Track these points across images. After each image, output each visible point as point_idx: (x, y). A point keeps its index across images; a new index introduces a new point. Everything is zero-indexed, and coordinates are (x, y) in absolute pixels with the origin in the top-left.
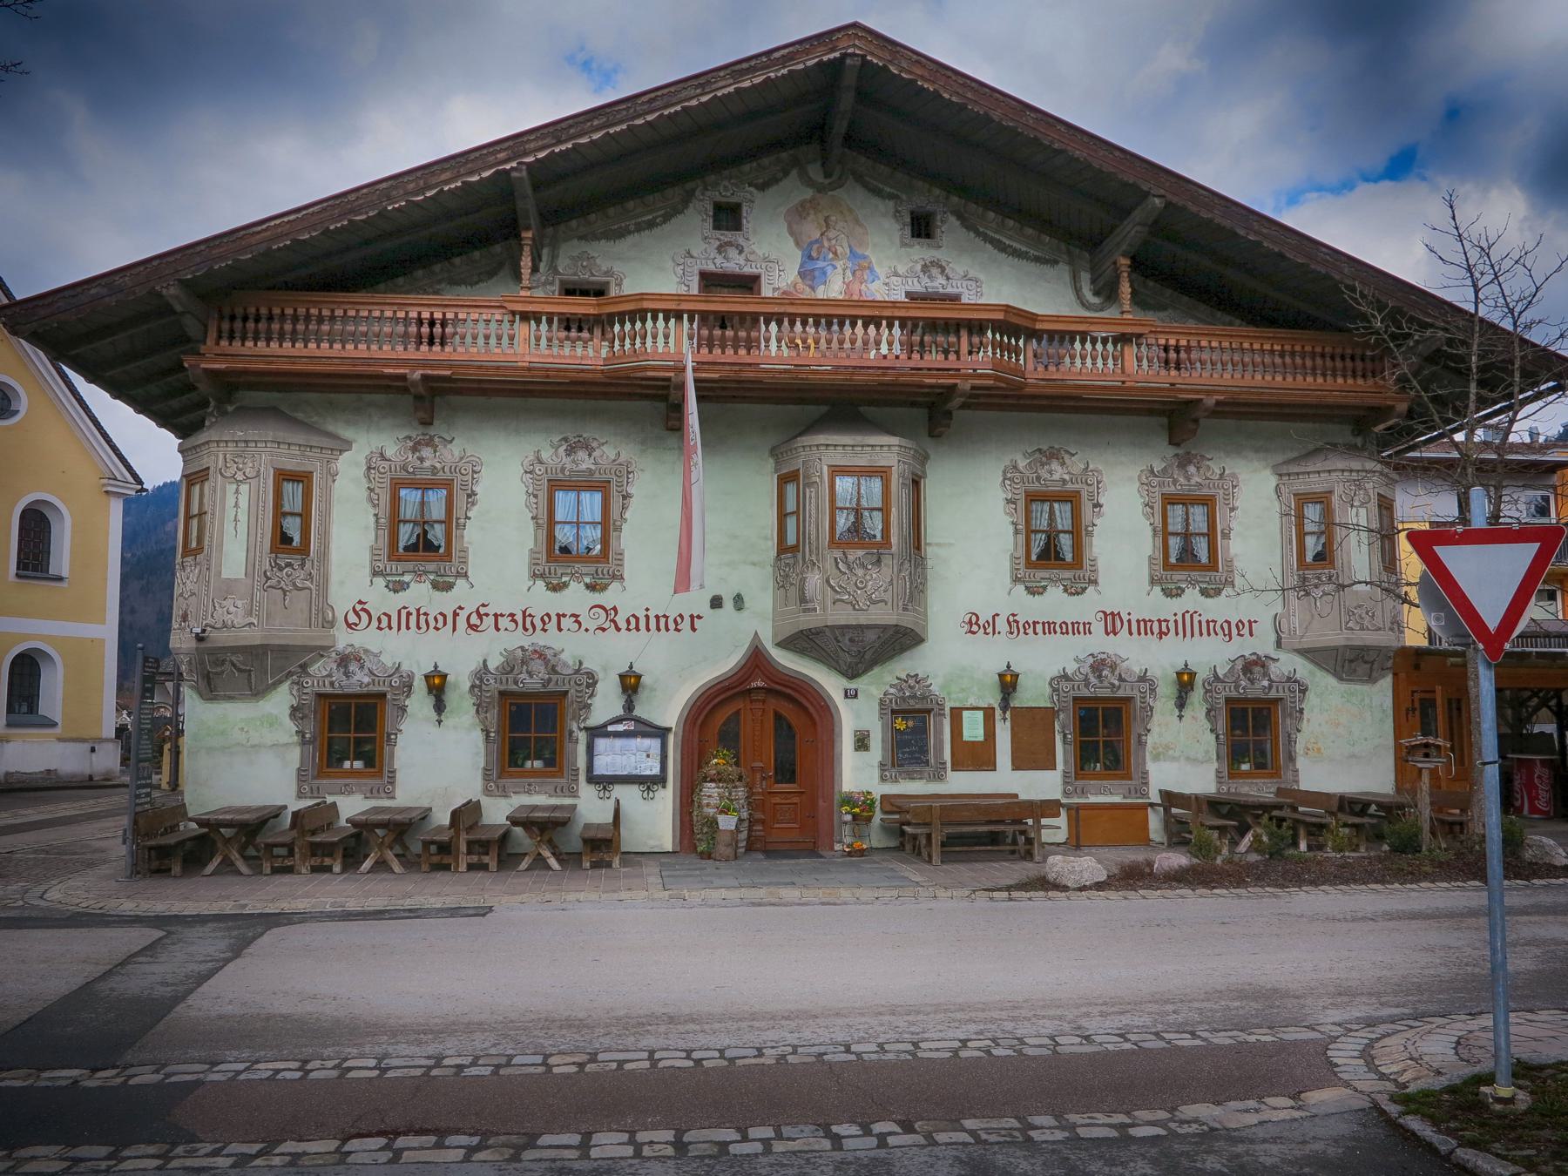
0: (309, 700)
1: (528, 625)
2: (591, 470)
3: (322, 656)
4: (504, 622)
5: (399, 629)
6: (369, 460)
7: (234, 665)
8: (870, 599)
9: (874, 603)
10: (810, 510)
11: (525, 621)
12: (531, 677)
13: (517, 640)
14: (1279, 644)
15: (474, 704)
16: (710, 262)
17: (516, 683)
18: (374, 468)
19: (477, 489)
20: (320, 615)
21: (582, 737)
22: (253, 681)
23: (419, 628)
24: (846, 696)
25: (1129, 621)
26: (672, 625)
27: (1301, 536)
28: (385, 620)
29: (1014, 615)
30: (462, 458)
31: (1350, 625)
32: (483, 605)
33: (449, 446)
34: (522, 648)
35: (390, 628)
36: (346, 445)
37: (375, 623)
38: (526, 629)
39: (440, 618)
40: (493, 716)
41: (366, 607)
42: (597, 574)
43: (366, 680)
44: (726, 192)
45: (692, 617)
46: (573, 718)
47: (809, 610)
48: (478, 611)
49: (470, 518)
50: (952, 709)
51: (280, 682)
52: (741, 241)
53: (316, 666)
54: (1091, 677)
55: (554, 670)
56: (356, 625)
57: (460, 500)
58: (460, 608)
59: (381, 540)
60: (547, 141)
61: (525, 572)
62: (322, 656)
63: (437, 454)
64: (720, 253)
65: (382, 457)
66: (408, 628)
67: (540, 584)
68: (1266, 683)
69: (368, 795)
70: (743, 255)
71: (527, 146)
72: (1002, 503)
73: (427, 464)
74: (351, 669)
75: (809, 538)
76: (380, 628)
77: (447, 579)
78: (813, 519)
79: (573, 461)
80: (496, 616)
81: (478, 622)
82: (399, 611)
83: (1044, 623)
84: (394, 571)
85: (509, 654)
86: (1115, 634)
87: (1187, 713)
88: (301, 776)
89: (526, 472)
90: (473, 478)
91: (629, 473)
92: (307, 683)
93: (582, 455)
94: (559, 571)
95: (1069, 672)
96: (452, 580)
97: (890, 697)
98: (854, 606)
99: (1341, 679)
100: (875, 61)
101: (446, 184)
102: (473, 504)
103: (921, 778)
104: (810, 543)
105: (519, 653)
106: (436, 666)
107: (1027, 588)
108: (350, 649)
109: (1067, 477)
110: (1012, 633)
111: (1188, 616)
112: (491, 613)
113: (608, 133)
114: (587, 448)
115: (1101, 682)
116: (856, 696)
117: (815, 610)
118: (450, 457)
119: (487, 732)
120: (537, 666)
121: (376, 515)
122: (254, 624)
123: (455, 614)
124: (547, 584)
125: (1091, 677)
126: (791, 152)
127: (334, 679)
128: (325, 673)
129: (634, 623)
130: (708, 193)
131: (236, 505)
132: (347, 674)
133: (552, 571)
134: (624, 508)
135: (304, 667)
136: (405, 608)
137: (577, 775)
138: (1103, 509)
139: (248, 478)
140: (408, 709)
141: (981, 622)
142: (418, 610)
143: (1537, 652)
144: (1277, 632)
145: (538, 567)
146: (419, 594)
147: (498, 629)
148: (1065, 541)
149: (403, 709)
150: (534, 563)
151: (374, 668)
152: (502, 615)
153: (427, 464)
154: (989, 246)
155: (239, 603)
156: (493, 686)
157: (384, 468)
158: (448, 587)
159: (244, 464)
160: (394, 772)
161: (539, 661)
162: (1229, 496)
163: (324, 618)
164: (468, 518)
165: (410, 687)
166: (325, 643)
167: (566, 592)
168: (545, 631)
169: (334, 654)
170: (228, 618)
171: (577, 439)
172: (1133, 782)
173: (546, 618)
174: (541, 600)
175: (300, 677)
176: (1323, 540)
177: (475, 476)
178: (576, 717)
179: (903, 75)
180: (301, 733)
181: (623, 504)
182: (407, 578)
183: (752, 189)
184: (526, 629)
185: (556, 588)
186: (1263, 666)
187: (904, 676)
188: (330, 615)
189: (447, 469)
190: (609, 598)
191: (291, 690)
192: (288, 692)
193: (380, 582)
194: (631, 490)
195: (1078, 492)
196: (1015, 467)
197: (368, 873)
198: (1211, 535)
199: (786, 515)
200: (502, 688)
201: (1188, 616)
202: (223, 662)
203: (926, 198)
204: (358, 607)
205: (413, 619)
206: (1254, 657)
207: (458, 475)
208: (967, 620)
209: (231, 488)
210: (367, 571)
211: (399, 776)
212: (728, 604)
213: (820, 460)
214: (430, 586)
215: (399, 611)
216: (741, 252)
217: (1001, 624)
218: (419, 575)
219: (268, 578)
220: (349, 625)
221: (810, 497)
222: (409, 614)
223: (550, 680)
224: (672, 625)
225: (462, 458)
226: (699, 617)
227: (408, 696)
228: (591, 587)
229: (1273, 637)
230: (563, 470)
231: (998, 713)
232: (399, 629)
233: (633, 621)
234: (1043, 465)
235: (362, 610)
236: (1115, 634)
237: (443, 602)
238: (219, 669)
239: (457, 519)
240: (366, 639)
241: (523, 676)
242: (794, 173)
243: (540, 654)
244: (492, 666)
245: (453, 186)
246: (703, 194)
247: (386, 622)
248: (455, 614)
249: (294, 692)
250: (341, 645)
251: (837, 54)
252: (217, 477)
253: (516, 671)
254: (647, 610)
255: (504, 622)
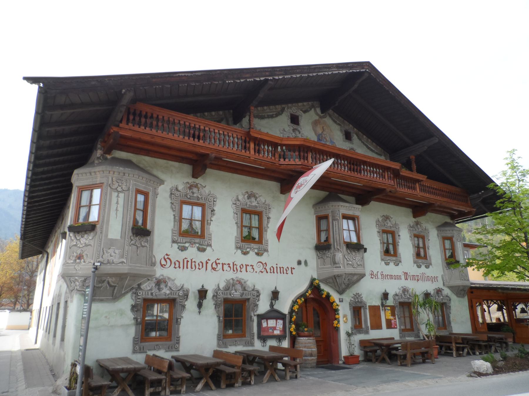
0: (140, 302)
1: (235, 269)
2: (256, 206)
3: (149, 280)
4: (226, 267)
5: (183, 268)
6: (171, 190)
7: (108, 283)
8: (357, 264)
9: (358, 265)
10: (336, 229)
11: (233, 267)
12: (236, 292)
13: (230, 275)
14: (444, 285)
15: (214, 304)
16: (291, 134)
17: (230, 295)
18: (173, 194)
19: (215, 208)
20: (150, 260)
21: (255, 319)
22: (115, 292)
23: (192, 268)
24: (340, 301)
25: (410, 275)
26: (285, 272)
27: (445, 249)
28: (177, 263)
29: (382, 272)
30: (209, 195)
31: (462, 279)
32: (218, 259)
33: (204, 189)
34: (233, 279)
35: (180, 268)
36: (162, 182)
37: (173, 265)
38: (234, 271)
39: (201, 264)
40: (222, 309)
41: (169, 257)
42: (259, 249)
43: (168, 292)
44: (294, 109)
45: (291, 268)
46: (252, 310)
47: (338, 267)
48: (216, 262)
49: (212, 221)
50: (369, 306)
51: (127, 292)
52: (299, 129)
53: (145, 285)
54: (402, 294)
55: (244, 289)
56: (165, 265)
57: (208, 212)
58: (209, 260)
59: (176, 226)
60: (282, 73)
61: (233, 246)
62: (149, 280)
63: (199, 191)
64: (293, 131)
65: (177, 189)
66: (187, 268)
67: (239, 251)
68: (442, 297)
69: (167, 350)
70: (300, 134)
71: (276, 72)
72: (377, 232)
73: (195, 195)
74: (161, 286)
75: (336, 240)
76: (175, 268)
77: (203, 247)
78: (337, 233)
79: (250, 202)
80: (223, 264)
81: (216, 267)
82: (184, 260)
83: (390, 275)
84: (181, 241)
85: (228, 281)
86: (407, 280)
87: (204, 311)
88: (135, 342)
89: (233, 204)
90: (214, 204)
91: (269, 209)
92: (140, 293)
93: (253, 199)
94: (246, 247)
95: (397, 293)
96: (205, 247)
97: (352, 301)
98: (353, 266)
99: (457, 296)
100: (373, 76)
101: (248, 79)
102: (214, 215)
103: (362, 333)
104: (336, 241)
105: (231, 281)
106: (203, 286)
107: (385, 263)
108: (161, 277)
109: (391, 225)
110: (382, 279)
111: (423, 274)
112: (221, 263)
113: (360, 71)
114: (255, 197)
115: (405, 296)
116: (342, 301)
117: (340, 267)
118: (204, 193)
119: (219, 317)
120: (238, 287)
121: (174, 215)
122: (124, 262)
123: (207, 263)
124: (242, 251)
125: (402, 294)
126: (312, 102)
127: (153, 291)
128: (149, 288)
129: (273, 270)
130: (289, 110)
131: (117, 203)
132: (159, 289)
133: (244, 246)
134: (268, 222)
135: (139, 285)
136: (186, 258)
137: (254, 336)
138: (401, 237)
139: (124, 190)
140: (186, 307)
141: (374, 274)
142: (192, 260)
143: (511, 288)
144: (443, 280)
145: (238, 244)
146: (192, 252)
147: (223, 270)
148: (391, 247)
149: (184, 307)
150: (237, 243)
151: (172, 286)
152: (225, 264)
153: (195, 195)
154: (365, 147)
155: (117, 251)
156: (221, 296)
157: (177, 194)
158: (203, 250)
159: (122, 183)
160: (179, 337)
161: (239, 285)
162: (428, 236)
163: (152, 261)
164: (211, 220)
165: (187, 296)
166: (152, 274)
167: (249, 255)
168: (241, 271)
169: (154, 279)
170: (111, 258)
171: (251, 193)
172: (415, 332)
173: (241, 266)
174: (240, 259)
175: (137, 290)
176: (451, 251)
177: (214, 203)
178: (253, 310)
179: (380, 82)
180: (136, 319)
181: (268, 221)
182: (187, 245)
183: (301, 112)
184: (234, 271)
185: (245, 253)
186: (441, 292)
187: (355, 294)
188: (154, 260)
189: (203, 198)
190: (264, 258)
191: (132, 296)
192: (130, 297)
193: (175, 246)
194: (270, 216)
195: (394, 231)
196: (379, 221)
197: (200, 391)
198: (424, 248)
199: (321, 231)
200: (225, 297)
201: (423, 274)
202: (104, 281)
203: (349, 127)
204: (166, 257)
205: (189, 263)
206: (439, 289)
207: (208, 202)
208: (370, 273)
209: (115, 194)
210: (170, 240)
211: (181, 339)
212: (303, 263)
213: (339, 211)
214: (197, 249)
215: (184, 260)
216: (300, 133)
217: (380, 276)
218: (192, 244)
219: (132, 240)
220: (162, 265)
221: (335, 225)
222: (188, 261)
223: (243, 294)
224: (285, 272)
225: (209, 195)
226: (294, 269)
227: (186, 300)
228: (258, 254)
229: (442, 283)
230: (246, 204)
231: (381, 307)
232: (183, 268)
233: (272, 269)
234: (385, 221)
235: (168, 258)
236: (407, 280)
237: (202, 257)
238: (100, 285)
239: (207, 221)
240: (168, 272)
241: (233, 291)
242: (313, 109)
243: (239, 282)
244: (221, 287)
245: (250, 80)
246: (287, 110)
247: (178, 265)
248: (207, 263)
249: (134, 298)
250: (158, 275)
251: (364, 70)
252: (107, 189)
253: (230, 289)
254: (277, 264)
255: (226, 267)
